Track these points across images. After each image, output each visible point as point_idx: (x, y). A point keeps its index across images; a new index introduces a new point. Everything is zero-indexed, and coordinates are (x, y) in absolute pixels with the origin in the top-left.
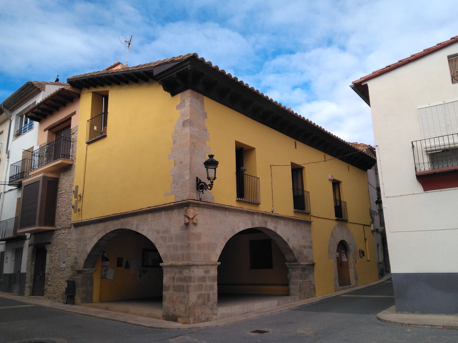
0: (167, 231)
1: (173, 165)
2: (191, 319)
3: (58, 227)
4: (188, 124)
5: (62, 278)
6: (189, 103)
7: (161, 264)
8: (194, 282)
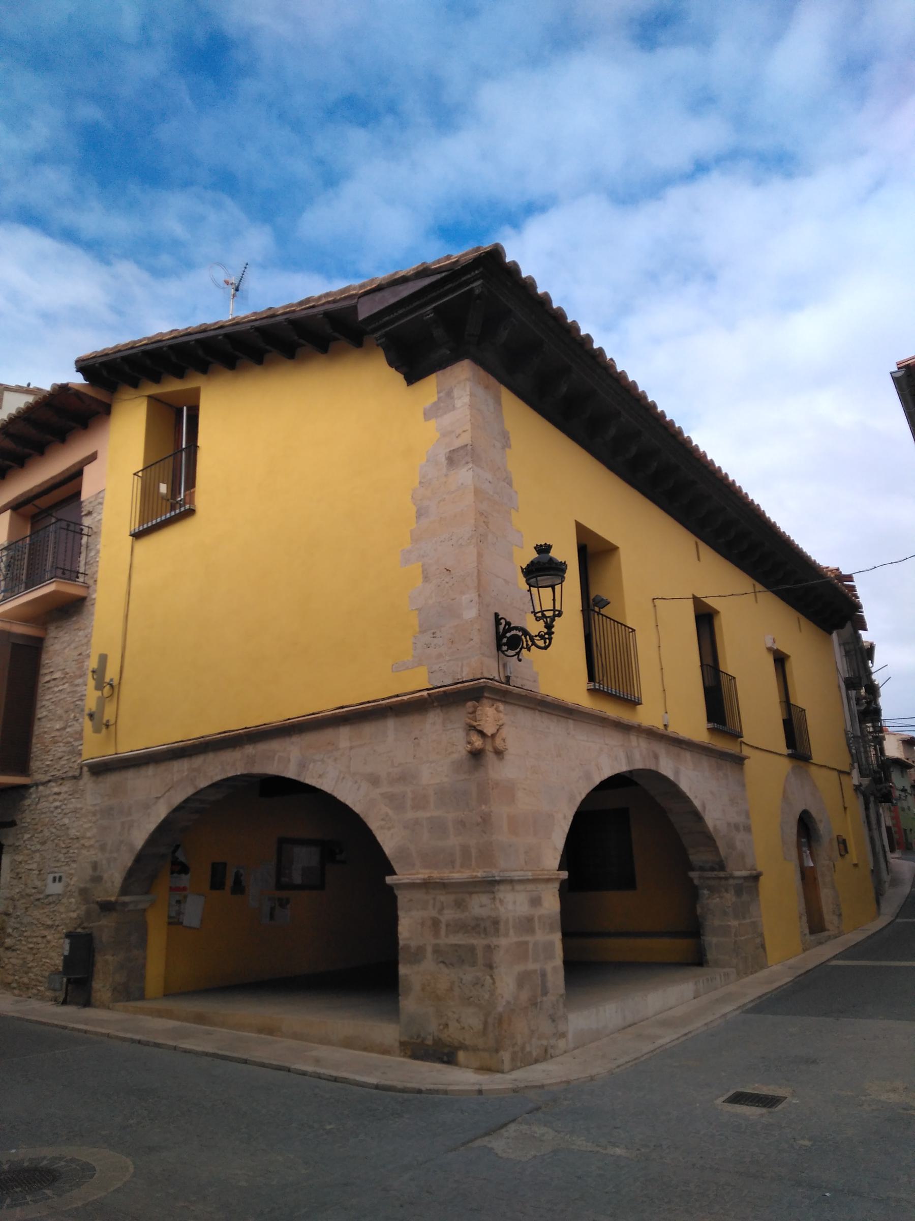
0: (403, 778)
1: (421, 580)
2: (506, 1056)
3: (39, 777)
4: (469, 459)
5: (50, 927)
6: (466, 399)
7: (389, 880)
8: (507, 935)
